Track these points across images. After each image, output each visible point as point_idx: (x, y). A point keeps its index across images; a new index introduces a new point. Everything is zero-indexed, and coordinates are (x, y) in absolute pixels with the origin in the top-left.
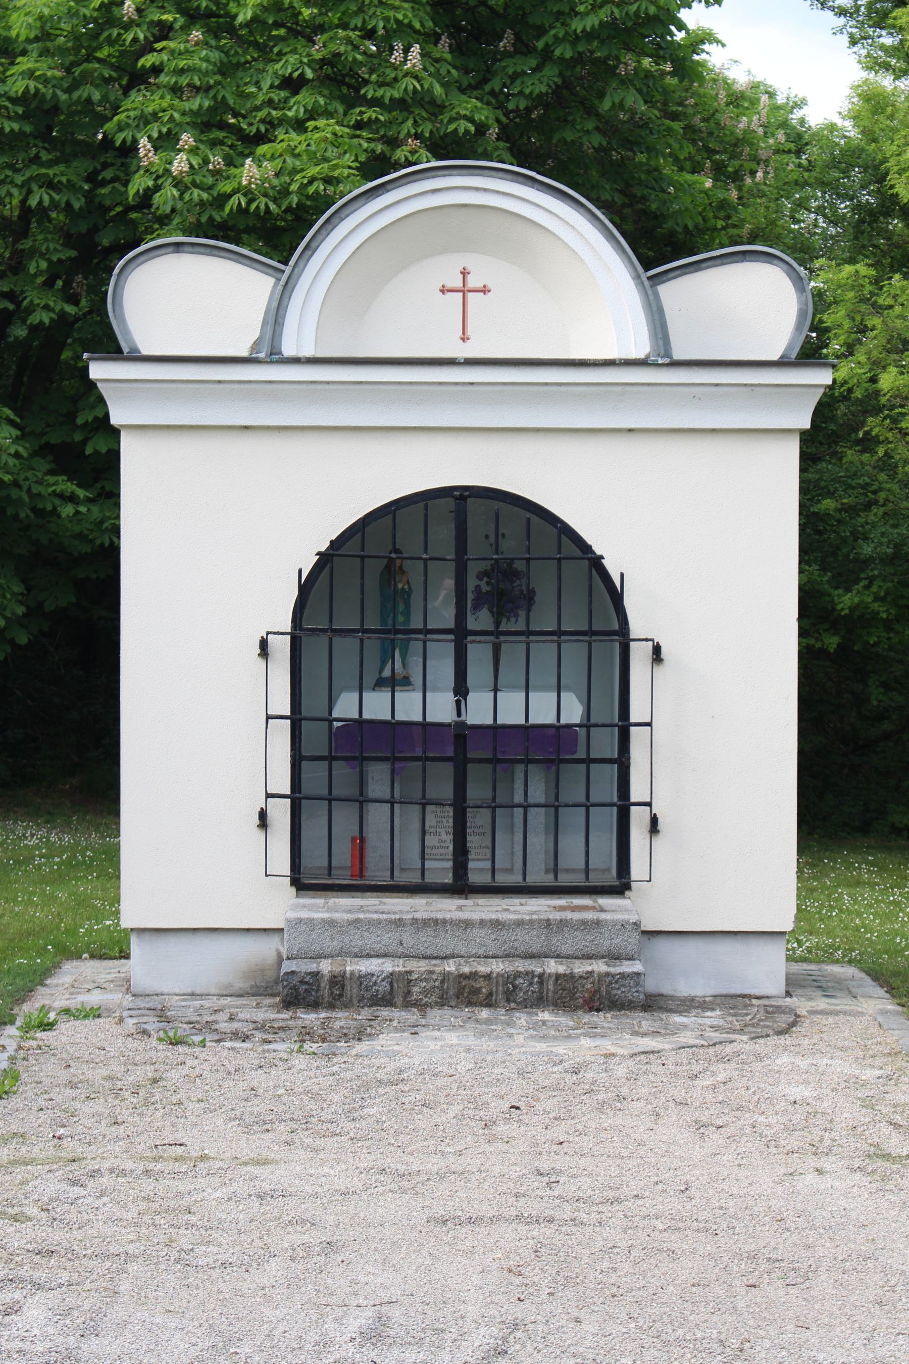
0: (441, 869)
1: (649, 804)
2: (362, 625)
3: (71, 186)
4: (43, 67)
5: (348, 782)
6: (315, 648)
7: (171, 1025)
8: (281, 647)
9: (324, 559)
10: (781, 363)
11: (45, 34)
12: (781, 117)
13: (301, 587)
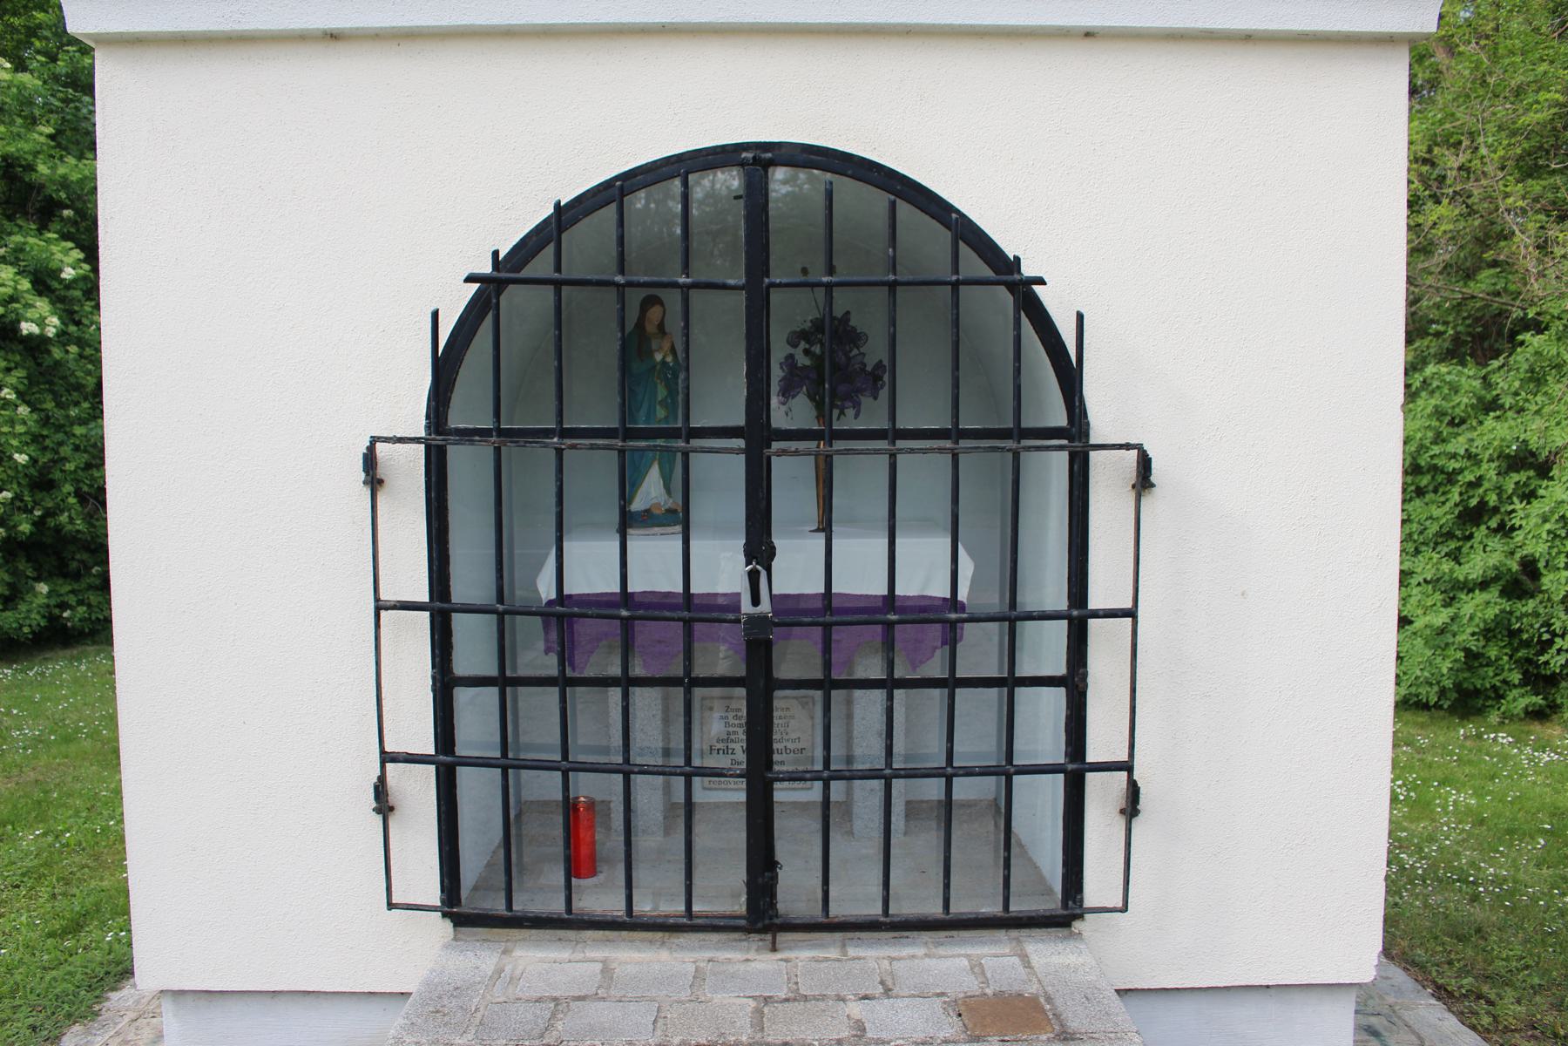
0: (724, 889)
1: (1127, 767)
2: (561, 422)
6: (469, 468)
8: (407, 468)
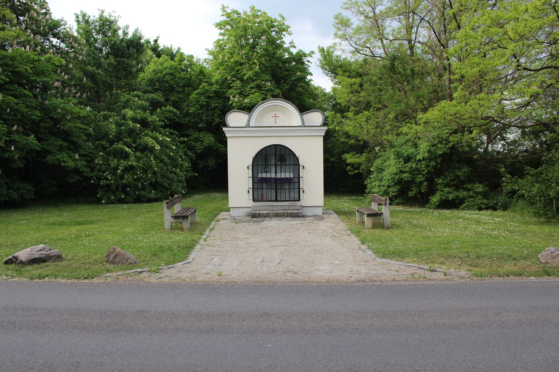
0: (274, 198)
3: (221, 103)
4: (218, 87)
5: (262, 186)
6: (255, 168)
7: (236, 220)
8: (251, 167)
9: (256, 155)
10: (320, 126)
11: (217, 82)
12: (322, 91)
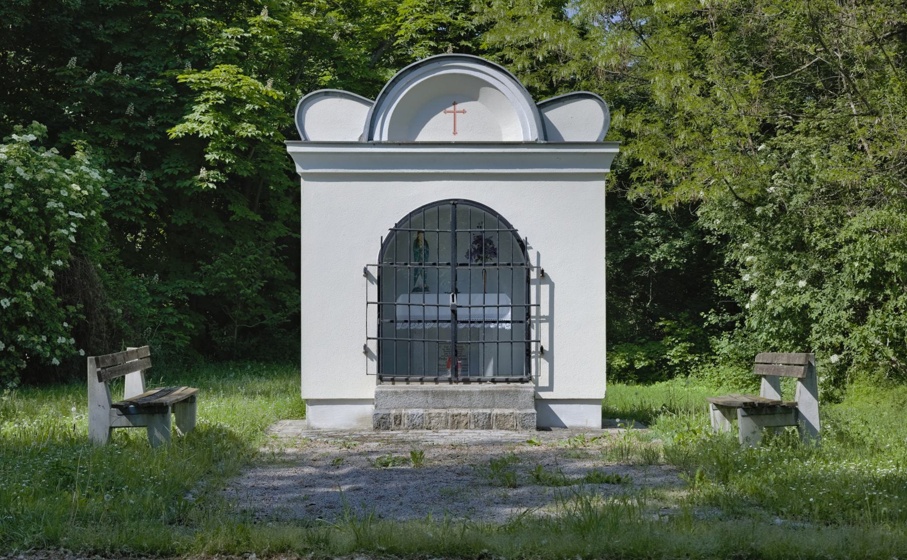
13: (382, 245)
